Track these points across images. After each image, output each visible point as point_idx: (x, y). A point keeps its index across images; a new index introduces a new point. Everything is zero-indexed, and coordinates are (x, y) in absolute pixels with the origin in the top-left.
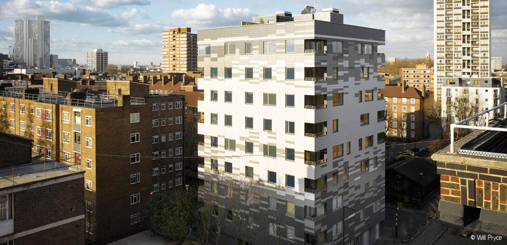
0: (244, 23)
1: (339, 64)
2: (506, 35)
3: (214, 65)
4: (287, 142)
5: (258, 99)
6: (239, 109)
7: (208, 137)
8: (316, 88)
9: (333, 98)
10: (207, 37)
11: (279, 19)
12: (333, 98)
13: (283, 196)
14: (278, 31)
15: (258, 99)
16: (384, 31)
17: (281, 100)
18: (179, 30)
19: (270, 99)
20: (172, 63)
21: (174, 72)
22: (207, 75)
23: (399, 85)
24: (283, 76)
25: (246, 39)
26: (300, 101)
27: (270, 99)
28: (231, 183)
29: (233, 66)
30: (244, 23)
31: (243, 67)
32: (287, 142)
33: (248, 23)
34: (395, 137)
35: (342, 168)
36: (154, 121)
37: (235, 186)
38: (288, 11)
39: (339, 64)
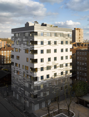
0: (57, 27)
1: (26, 40)
2: (88, 32)
3: (67, 40)
4: (41, 65)
5: (52, 51)
6: (59, 55)
7: (69, 63)
8: (34, 48)
9: (28, 51)
10: (69, 31)
11: (46, 25)
12: (28, 51)
13: (46, 82)
14: (44, 29)
15: (52, 51)
16: (12, 29)
17: (45, 51)
18: (78, 29)
19: (49, 51)
20: (78, 39)
21: (79, 42)
22: (64, 44)
23: (7, 47)
24: (54, 43)
25: (56, 32)
26: (39, 52)
27: (49, 51)
28: (61, 78)
29: (44, 41)
30: (57, 27)
31: (48, 41)
32: (41, 65)
33: (56, 27)
34: (8, 64)
35: (81, 78)
36: (86, 58)
37: (60, 79)
38: (27, 22)
39: (26, 40)
